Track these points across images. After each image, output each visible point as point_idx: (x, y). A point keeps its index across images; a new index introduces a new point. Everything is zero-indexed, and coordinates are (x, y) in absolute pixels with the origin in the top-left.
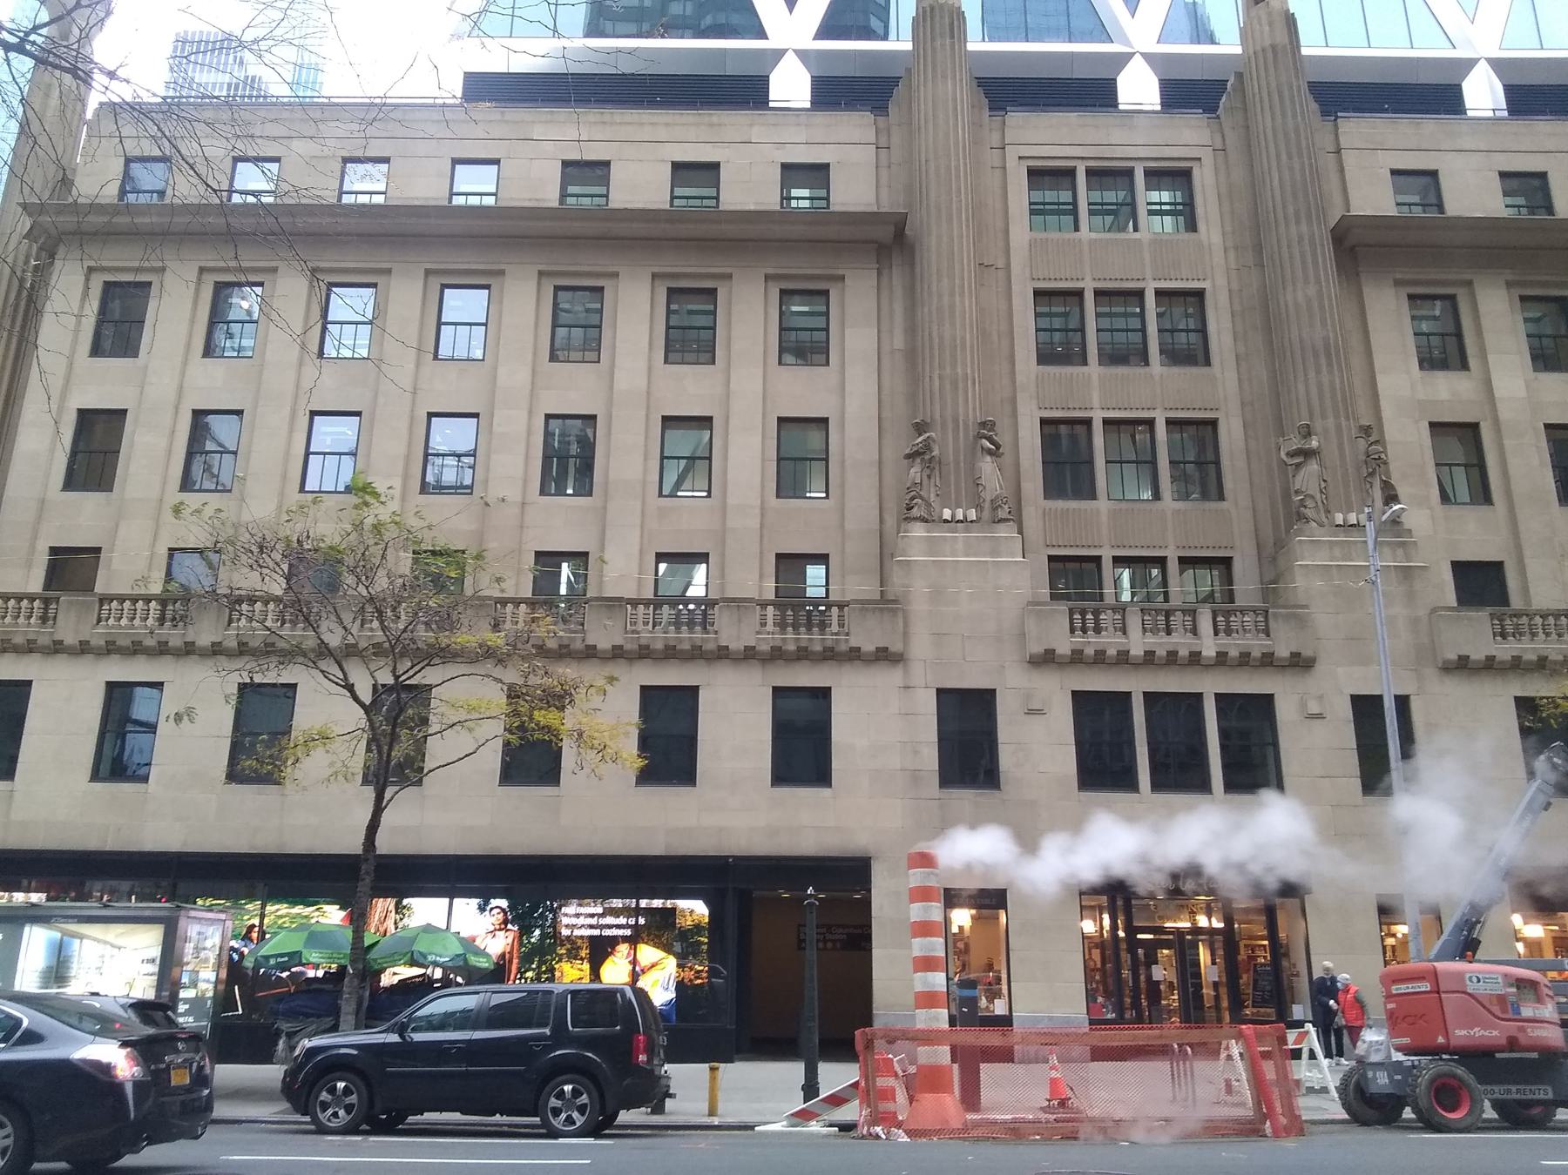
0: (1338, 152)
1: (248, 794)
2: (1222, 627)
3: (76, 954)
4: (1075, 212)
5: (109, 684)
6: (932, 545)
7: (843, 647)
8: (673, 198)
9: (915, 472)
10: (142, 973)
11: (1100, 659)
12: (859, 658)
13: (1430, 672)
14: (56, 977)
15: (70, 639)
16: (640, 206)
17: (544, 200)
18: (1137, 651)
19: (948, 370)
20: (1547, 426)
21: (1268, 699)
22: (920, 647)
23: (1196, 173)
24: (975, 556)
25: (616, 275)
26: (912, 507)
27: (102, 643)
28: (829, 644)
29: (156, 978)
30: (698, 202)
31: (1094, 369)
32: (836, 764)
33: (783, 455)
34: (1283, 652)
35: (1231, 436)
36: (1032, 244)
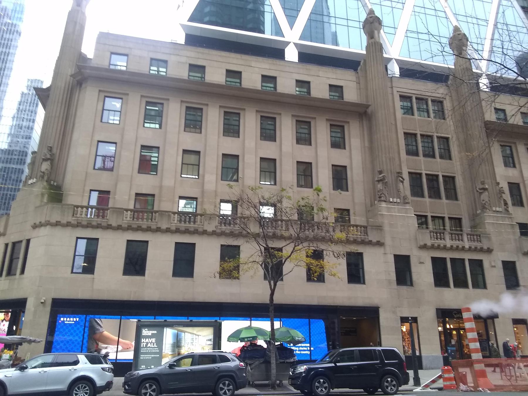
0: (392, 88)
1: (181, 281)
2: (135, 217)
3: (183, 338)
4: (428, 112)
5: (128, 241)
6: (389, 209)
7: (367, 240)
8: (189, 75)
9: (380, 186)
10: (207, 344)
11: (438, 248)
12: (371, 244)
13: (520, 255)
14: (177, 346)
15: (114, 224)
16: (287, 92)
17: (257, 87)
18: (448, 245)
19: (388, 155)
20: (333, 165)
21: (481, 261)
22: (388, 241)
23: (445, 102)
24: (401, 214)
25: (244, 109)
26: (381, 197)
27: (126, 226)
28: (363, 239)
29: (212, 346)
30: (234, 84)
31: (421, 158)
32: (366, 277)
33: (183, 163)
34: (485, 247)
35: (459, 182)
36: (402, 118)
